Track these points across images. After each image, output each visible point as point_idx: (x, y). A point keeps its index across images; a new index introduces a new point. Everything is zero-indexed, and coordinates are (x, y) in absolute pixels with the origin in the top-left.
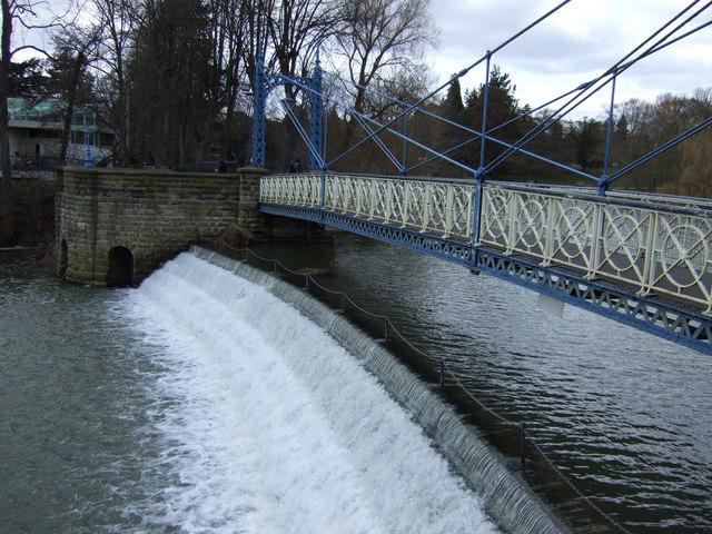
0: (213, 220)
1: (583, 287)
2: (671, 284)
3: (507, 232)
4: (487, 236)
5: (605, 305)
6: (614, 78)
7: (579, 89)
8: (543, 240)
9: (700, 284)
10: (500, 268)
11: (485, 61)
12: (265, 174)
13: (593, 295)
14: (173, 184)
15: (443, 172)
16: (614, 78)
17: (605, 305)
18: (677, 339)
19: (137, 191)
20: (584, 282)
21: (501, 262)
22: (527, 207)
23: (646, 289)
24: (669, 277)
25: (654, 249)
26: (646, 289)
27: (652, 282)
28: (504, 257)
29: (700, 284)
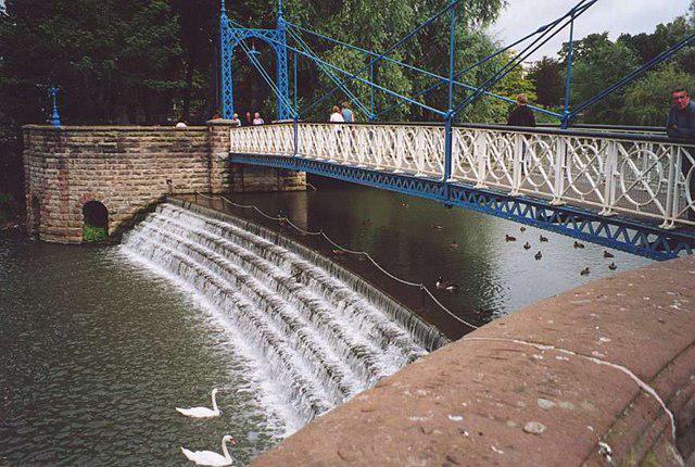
0: (188, 174)
1: (549, 213)
2: (633, 205)
3: (602, 188)
4: (458, 173)
5: (570, 226)
6: (571, 21)
7: (539, 31)
8: (602, 188)
9: (657, 201)
10: (472, 201)
11: (569, 25)
12: (234, 126)
13: (559, 219)
14: (143, 138)
15: (417, 118)
16: (571, 21)
17: (570, 226)
18: (639, 251)
19: (108, 147)
20: (550, 208)
21: (413, 183)
22: (634, 157)
23: (669, 222)
24: (627, 196)
25: (677, 182)
26: (607, 209)
27: (675, 214)
28: (475, 190)
29: (657, 201)
